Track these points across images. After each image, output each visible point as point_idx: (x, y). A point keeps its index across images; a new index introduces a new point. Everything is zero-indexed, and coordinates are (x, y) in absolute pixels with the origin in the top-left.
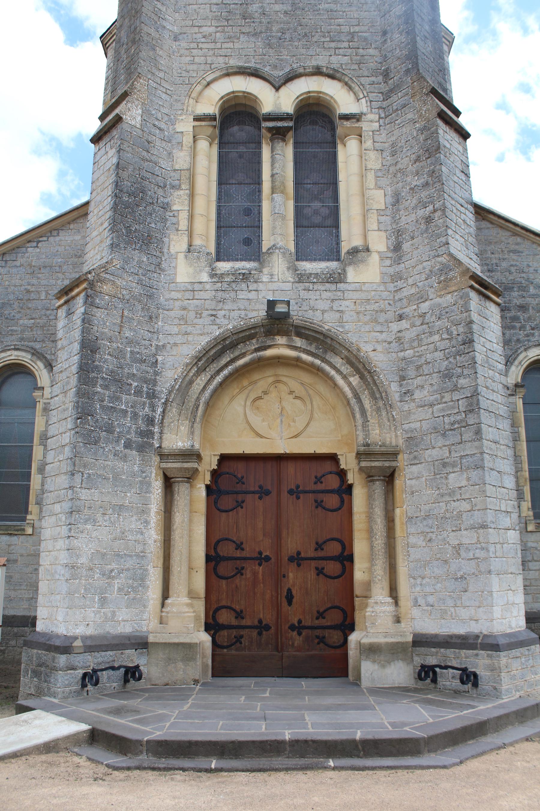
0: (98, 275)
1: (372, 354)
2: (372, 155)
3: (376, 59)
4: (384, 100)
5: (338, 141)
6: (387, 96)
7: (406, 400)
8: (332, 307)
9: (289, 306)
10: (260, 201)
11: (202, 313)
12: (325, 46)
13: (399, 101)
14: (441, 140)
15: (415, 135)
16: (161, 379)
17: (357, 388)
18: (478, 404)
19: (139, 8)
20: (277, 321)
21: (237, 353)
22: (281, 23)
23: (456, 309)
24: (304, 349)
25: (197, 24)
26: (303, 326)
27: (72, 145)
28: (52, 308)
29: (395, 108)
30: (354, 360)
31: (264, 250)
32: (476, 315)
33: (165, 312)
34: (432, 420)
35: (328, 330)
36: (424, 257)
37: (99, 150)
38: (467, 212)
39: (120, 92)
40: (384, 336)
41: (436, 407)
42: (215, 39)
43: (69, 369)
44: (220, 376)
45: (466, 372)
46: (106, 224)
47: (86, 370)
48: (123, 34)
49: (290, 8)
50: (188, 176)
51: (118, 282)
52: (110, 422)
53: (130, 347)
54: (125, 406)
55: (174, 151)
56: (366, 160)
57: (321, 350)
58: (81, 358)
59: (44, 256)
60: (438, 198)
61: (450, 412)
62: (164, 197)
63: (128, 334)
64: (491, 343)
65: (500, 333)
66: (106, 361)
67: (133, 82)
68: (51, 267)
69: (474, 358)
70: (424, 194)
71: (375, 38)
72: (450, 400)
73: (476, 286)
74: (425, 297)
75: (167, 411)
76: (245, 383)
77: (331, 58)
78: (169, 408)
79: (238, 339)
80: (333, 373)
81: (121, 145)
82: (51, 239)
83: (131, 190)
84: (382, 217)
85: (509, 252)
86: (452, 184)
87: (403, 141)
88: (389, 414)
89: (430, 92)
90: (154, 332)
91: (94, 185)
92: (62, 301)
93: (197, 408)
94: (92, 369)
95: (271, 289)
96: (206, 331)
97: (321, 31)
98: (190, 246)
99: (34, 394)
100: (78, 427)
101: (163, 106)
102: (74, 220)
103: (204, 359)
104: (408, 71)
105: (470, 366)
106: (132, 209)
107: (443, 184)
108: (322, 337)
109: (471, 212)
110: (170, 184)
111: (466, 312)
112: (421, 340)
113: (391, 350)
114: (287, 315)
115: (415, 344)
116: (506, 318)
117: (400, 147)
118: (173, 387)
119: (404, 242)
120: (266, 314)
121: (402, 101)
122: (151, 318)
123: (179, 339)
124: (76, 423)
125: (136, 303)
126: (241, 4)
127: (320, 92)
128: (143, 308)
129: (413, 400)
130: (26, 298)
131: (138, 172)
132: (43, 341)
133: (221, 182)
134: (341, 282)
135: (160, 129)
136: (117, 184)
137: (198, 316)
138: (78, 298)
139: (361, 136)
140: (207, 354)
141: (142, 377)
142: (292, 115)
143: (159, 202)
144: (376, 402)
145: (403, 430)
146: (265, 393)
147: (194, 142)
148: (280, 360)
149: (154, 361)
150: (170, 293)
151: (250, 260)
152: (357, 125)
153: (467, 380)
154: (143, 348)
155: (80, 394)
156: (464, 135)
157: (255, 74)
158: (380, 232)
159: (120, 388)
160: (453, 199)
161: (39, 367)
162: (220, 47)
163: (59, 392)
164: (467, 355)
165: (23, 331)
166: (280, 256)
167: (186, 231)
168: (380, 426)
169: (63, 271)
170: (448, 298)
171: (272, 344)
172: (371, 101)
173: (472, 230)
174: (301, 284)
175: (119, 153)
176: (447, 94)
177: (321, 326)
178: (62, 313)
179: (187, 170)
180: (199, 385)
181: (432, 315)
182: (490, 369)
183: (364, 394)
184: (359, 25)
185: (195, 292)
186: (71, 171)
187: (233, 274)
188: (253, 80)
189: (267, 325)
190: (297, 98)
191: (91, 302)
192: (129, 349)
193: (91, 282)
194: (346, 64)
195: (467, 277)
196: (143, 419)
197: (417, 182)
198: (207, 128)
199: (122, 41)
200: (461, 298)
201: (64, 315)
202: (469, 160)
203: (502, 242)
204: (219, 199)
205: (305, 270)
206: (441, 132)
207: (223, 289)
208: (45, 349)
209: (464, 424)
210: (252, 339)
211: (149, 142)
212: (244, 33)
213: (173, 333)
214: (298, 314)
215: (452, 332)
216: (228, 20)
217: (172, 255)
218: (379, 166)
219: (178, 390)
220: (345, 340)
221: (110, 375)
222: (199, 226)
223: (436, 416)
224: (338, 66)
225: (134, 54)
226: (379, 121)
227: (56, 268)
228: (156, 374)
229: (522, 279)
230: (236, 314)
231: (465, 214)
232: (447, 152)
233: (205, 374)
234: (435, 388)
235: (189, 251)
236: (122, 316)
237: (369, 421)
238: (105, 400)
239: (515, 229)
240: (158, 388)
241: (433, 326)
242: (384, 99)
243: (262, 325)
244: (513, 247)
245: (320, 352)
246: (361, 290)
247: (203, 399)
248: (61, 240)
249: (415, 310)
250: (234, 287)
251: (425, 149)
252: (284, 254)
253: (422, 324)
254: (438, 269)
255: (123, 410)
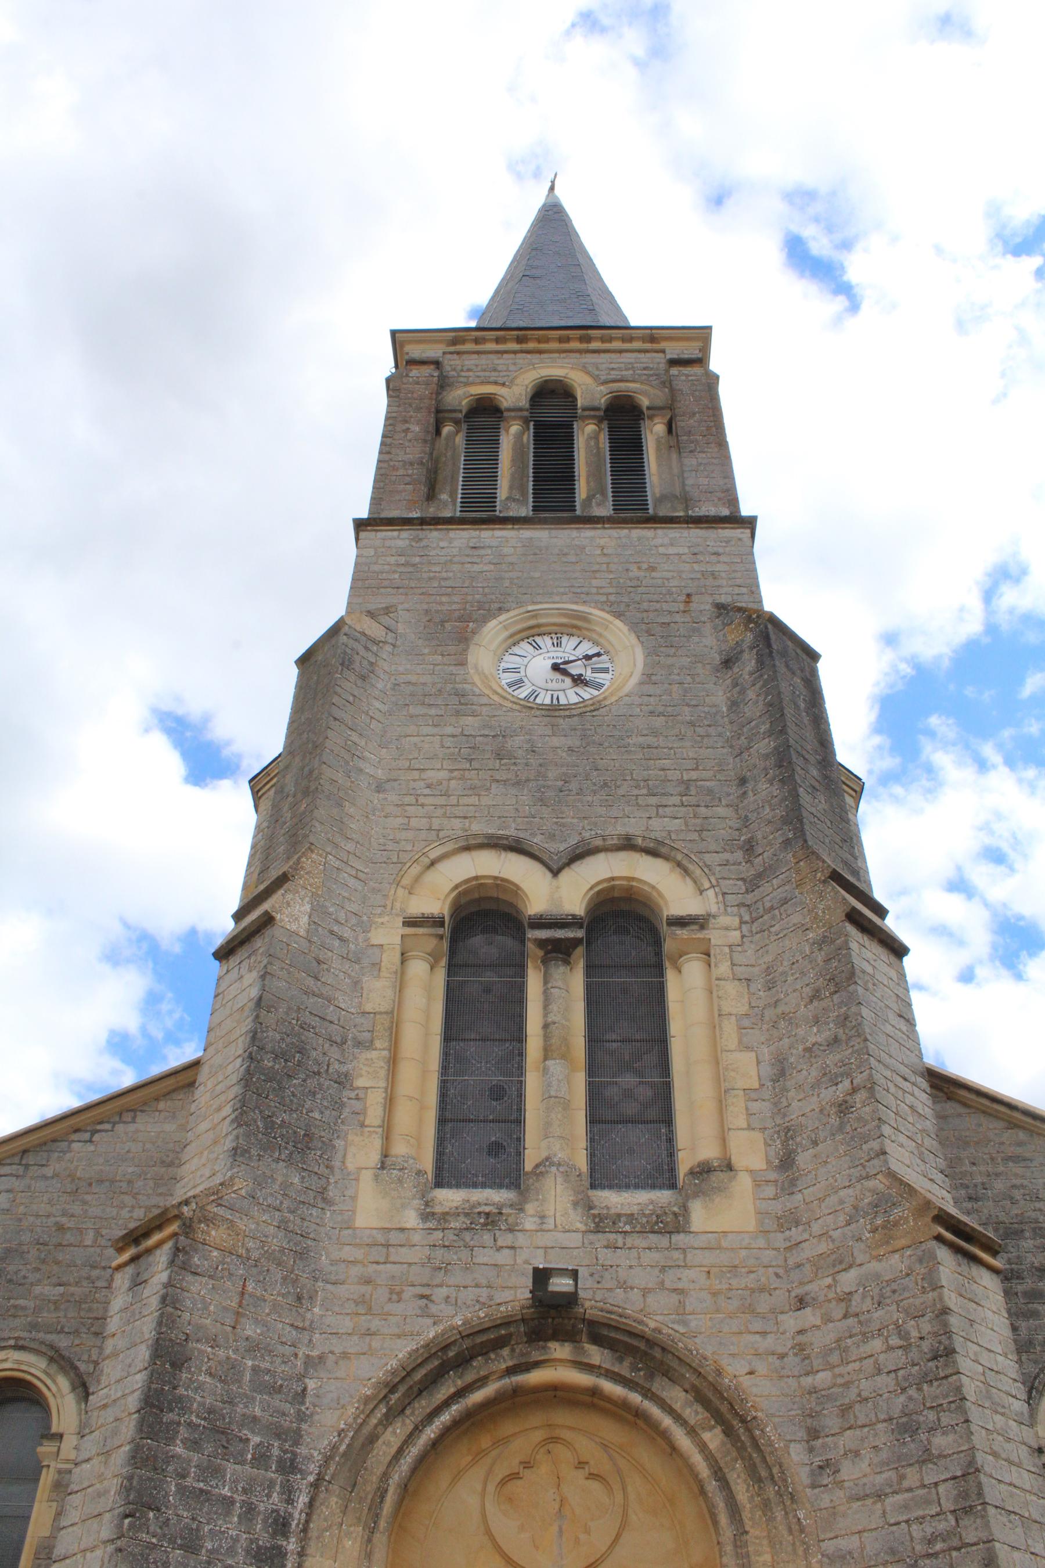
0: (202, 1208)
1: (746, 1381)
2: (731, 988)
3: (730, 823)
4: (747, 892)
5: (667, 964)
6: (752, 884)
7: (825, 1482)
8: (662, 1283)
9: (576, 1280)
10: (521, 1070)
11: (403, 1291)
12: (640, 802)
13: (775, 893)
14: (856, 960)
15: (808, 953)
16: (311, 1430)
17: (718, 1456)
18: (980, 1494)
19: (321, 740)
20: (551, 1314)
21: (470, 1377)
22: (562, 766)
23: (912, 1285)
24: (607, 1370)
25: (417, 766)
26: (605, 1321)
27: (177, 949)
28: (103, 1264)
29: (768, 905)
30: (710, 1394)
31: (528, 1166)
32: (953, 1295)
33: (329, 1286)
34: (884, 1532)
35: (654, 1330)
36: (839, 1180)
37: (228, 971)
38: (916, 1091)
39: (274, 874)
40: (769, 1342)
41: (890, 1500)
42: (447, 791)
43: (123, 1401)
44: (434, 1426)
45: (946, 1419)
46: (227, 1110)
47: (157, 1406)
48: (289, 780)
49: (578, 743)
50: (387, 1024)
51: (241, 1224)
52: (194, 1526)
53: (253, 1360)
54: (231, 1489)
55: (365, 979)
56: (719, 997)
57: (642, 1373)
58: (150, 1380)
59: (101, 1160)
60: (859, 1067)
61: (921, 1513)
62: (341, 1063)
63: (250, 1330)
64: (992, 1355)
65: (1007, 1332)
66: (200, 1387)
67: (299, 858)
68: (112, 1182)
69: (959, 1389)
70: (832, 1059)
71: (725, 789)
72: (918, 1484)
73: (948, 1235)
74: (847, 1260)
75: (318, 1504)
76: (485, 1441)
77: (650, 822)
78: (322, 1496)
79: (473, 1347)
80: (667, 1421)
81: (269, 966)
82: (120, 1127)
83: (280, 1047)
84: (755, 1104)
85: (1007, 1159)
86: (882, 1039)
87: (785, 963)
88: (791, 1516)
89: (830, 877)
90: (304, 1329)
91: (212, 1034)
92: (126, 1256)
93: (382, 1498)
94: (170, 1403)
95: (540, 1244)
96: (408, 1328)
97: (632, 779)
98: (386, 1156)
99: (40, 1449)
100: (123, 1536)
101: (349, 900)
102: (167, 1095)
103: (402, 1389)
104: (787, 843)
105: (953, 1405)
106: (279, 1083)
107: (866, 1040)
108: (642, 1345)
109: (924, 1091)
110: (354, 1038)
111: (933, 1290)
112: (846, 1350)
113: (784, 1372)
114: (571, 1299)
115: (834, 1358)
116: (1016, 1294)
117: (782, 974)
118: (334, 1448)
119: (799, 1150)
120: (530, 1296)
121: (779, 894)
122: (299, 1298)
123: (353, 1345)
124: (120, 1526)
125: (273, 1267)
126: (493, 736)
127: (633, 879)
128: (285, 1278)
129: (839, 1484)
130: (54, 1241)
131: (294, 1015)
132: (77, 1332)
133: (449, 1036)
134: (678, 1232)
135: (341, 939)
136: (254, 1036)
137: (395, 1297)
138: (158, 1252)
139: (709, 956)
140: (408, 1379)
141: (271, 1424)
142: (581, 918)
143: (331, 1070)
144: (760, 1488)
145: (823, 1555)
146: (527, 1465)
147: (403, 962)
148: (559, 1393)
149: (299, 1389)
150: (340, 1250)
151: (500, 1186)
152: (700, 935)
153: (950, 1438)
154: (279, 1360)
155: (139, 1458)
156: (898, 950)
157: (517, 847)
158: (752, 1133)
159: (224, 1447)
160: (886, 1066)
161: (59, 1389)
162: (455, 802)
163: (94, 1452)
164: (944, 1381)
165: (37, 1310)
166: (559, 1180)
167: (379, 1127)
168: (772, 1544)
169: (135, 1191)
170: (893, 1261)
171: (542, 1358)
172: (724, 894)
173: (930, 1125)
174: (600, 1236)
175: (264, 980)
176: (859, 880)
177: (641, 1322)
178: (122, 1280)
179: (386, 1013)
180: (388, 1444)
181: (864, 1297)
182: (996, 1412)
183: (734, 1469)
184: (697, 769)
185: (390, 1248)
186: (170, 995)
187: (467, 1215)
188: (513, 858)
189: (533, 1319)
190: (591, 888)
191: (184, 1263)
192: (250, 1363)
193: (188, 1222)
194: (677, 832)
195: (928, 1219)
196: (265, 1521)
197: (816, 1036)
198: (427, 940)
199: (286, 790)
200: (920, 1261)
201: (127, 1284)
202: (919, 1028)
203: (990, 1141)
204: (444, 1069)
205: (608, 1208)
206: (854, 946)
207: (446, 1244)
208: (77, 1349)
209: (956, 1542)
210: (501, 1348)
211: (319, 962)
212: (498, 781)
213: (341, 1331)
214: (595, 1298)
215: (908, 1333)
216: (471, 761)
217: (349, 1174)
218: (743, 1009)
219: (345, 1454)
220: (690, 1351)
221: (205, 1419)
222: (404, 1117)
223: (892, 1521)
224: (664, 834)
225: (304, 813)
226: (740, 928)
227: (121, 1184)
228: (301, 1417)
229: (1038, 1213)
230: (470, 1294)
231: (913, 1095)
232: (868, 981)
233: (403, 1421)
234: (885, 1456)
235: (383, 1168)
236: (243, 1294)
237: (747, 1532)
238: (189, 1473)
239: (1011, 1117)
240: (302, 1450)
241: (869, 1321)
242: (747, 890)
243: (523, 1320)
244: (1011, 1150)
245: (640, 1376)
246: (720, 1248)
247: (396, 1477)
248: (137, 1131)
249: (829, 1287)
250: (468, 1238)
251: (828, 977)
252: (566, 1175)
253: (845, 1317)
254: (869, 1204)
255: (225, 1498)
